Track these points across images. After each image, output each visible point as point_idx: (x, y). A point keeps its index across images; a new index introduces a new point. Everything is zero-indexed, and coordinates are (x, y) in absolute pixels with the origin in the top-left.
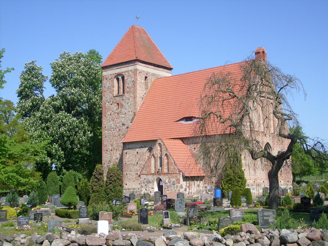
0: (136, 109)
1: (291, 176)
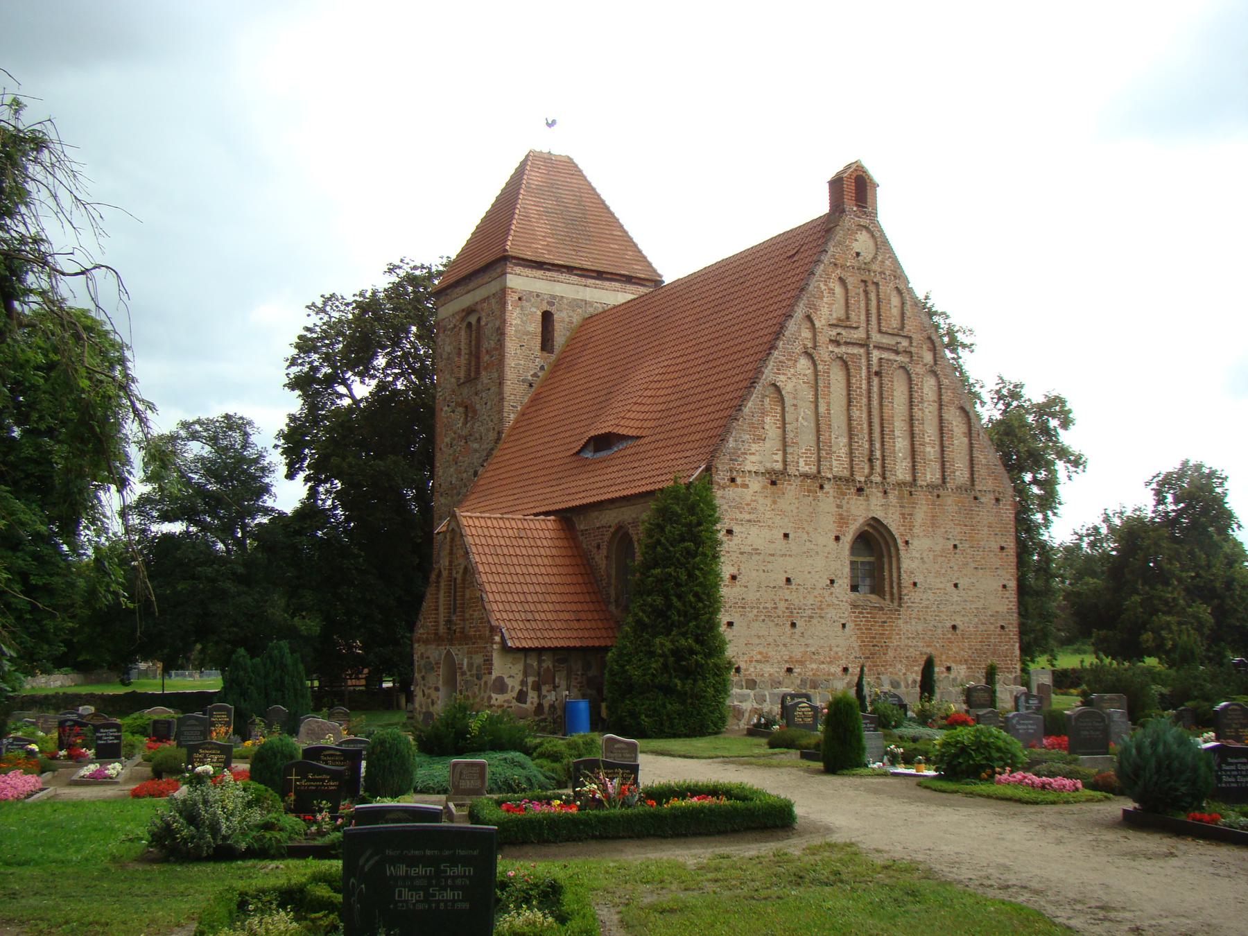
0: (501, 420)
1: (1013, 646)
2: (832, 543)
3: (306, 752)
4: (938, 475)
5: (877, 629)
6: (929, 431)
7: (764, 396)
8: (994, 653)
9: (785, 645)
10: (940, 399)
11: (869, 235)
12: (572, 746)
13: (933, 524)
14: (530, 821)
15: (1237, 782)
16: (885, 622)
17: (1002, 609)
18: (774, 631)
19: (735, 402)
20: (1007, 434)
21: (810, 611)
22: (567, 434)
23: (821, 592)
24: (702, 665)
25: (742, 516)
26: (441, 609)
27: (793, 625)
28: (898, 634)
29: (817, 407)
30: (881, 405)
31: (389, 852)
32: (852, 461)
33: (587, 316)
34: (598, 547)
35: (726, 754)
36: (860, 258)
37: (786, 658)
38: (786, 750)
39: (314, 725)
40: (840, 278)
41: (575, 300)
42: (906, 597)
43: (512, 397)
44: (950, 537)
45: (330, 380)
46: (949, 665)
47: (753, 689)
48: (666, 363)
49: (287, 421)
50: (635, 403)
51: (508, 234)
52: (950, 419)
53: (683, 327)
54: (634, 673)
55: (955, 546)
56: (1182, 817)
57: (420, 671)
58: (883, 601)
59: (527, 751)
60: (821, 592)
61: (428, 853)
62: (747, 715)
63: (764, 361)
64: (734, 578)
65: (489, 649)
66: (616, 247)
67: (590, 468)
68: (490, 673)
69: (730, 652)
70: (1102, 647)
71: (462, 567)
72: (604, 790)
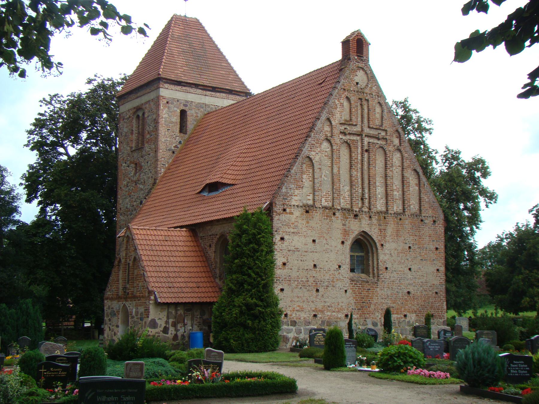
0: (156, 172)
1: (443, 303)
2: (340, 246)
3: (48, 358)
4: (401, 207)
5: (365, 293)
6: (396, 183)
7: (303, 163)
8: (431, 308)
9: (312, 302)
10: (403, 165)
11: (364, 73)
12: (191, 355)
13: (397, 235)
14: (165, 389)
15: (518, 373)
16: (369, 289)
17: (436, 282)
18: (307, 294)
19: (287, 166)
20: (450, 181)
21: (327, 283)
22: (194, 181)
23: (333, 272)
24: (263, 312)
25: (289, 230)
26: (121, 281)
27: (317, 290)
28: (377, 296)
29: (332, 169)
30: (369, 169)
31: (98, 391)
32: (352, 199)
33: (206, 113)
34: (210, 246)
35: (275, 360)
36: (359, 86)
37: (313, 309)
38: (308, 359)
39: (49, 346)
40: (347, 98)
41: (199, 103)
42: (381, 276)
43: (163, 159)
44: (407, 242)
45: (54, 145)
46: (405, 314)
47: (295, 326)
48: (249, 143)
49: (28, 169)
50: (232, 165)
51: (163, 55)
52: (408, 176)
53: (260, 122)
54: (227, 317)
55: (410, 247)
56: (487, 389)
57: (108, 316)
58: (368, 278)
59: (166, 358)
60: (333, 272)
61: (116, 391)
62: (291, 340)
63: (304, 143)
64: (284, 264)
65: (147, 303)
66: (224, 72)
67: (206, 201)
68: (148, 317)
69: (281, 305)
70: (501, 305)
71: (133, 257)
72: (203, 375)
